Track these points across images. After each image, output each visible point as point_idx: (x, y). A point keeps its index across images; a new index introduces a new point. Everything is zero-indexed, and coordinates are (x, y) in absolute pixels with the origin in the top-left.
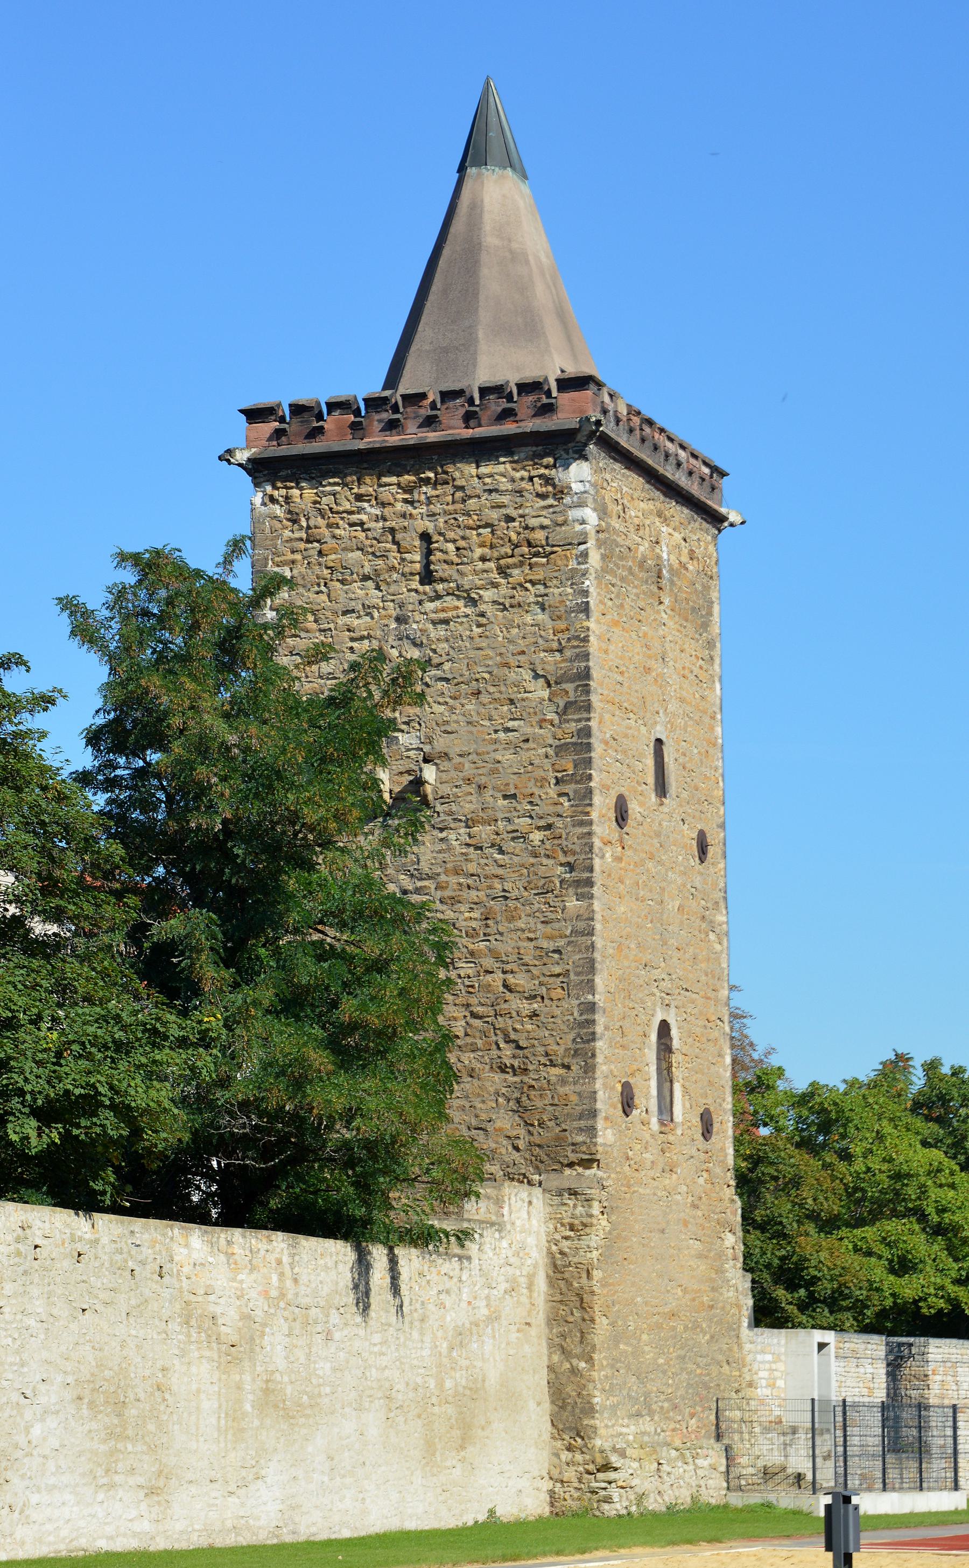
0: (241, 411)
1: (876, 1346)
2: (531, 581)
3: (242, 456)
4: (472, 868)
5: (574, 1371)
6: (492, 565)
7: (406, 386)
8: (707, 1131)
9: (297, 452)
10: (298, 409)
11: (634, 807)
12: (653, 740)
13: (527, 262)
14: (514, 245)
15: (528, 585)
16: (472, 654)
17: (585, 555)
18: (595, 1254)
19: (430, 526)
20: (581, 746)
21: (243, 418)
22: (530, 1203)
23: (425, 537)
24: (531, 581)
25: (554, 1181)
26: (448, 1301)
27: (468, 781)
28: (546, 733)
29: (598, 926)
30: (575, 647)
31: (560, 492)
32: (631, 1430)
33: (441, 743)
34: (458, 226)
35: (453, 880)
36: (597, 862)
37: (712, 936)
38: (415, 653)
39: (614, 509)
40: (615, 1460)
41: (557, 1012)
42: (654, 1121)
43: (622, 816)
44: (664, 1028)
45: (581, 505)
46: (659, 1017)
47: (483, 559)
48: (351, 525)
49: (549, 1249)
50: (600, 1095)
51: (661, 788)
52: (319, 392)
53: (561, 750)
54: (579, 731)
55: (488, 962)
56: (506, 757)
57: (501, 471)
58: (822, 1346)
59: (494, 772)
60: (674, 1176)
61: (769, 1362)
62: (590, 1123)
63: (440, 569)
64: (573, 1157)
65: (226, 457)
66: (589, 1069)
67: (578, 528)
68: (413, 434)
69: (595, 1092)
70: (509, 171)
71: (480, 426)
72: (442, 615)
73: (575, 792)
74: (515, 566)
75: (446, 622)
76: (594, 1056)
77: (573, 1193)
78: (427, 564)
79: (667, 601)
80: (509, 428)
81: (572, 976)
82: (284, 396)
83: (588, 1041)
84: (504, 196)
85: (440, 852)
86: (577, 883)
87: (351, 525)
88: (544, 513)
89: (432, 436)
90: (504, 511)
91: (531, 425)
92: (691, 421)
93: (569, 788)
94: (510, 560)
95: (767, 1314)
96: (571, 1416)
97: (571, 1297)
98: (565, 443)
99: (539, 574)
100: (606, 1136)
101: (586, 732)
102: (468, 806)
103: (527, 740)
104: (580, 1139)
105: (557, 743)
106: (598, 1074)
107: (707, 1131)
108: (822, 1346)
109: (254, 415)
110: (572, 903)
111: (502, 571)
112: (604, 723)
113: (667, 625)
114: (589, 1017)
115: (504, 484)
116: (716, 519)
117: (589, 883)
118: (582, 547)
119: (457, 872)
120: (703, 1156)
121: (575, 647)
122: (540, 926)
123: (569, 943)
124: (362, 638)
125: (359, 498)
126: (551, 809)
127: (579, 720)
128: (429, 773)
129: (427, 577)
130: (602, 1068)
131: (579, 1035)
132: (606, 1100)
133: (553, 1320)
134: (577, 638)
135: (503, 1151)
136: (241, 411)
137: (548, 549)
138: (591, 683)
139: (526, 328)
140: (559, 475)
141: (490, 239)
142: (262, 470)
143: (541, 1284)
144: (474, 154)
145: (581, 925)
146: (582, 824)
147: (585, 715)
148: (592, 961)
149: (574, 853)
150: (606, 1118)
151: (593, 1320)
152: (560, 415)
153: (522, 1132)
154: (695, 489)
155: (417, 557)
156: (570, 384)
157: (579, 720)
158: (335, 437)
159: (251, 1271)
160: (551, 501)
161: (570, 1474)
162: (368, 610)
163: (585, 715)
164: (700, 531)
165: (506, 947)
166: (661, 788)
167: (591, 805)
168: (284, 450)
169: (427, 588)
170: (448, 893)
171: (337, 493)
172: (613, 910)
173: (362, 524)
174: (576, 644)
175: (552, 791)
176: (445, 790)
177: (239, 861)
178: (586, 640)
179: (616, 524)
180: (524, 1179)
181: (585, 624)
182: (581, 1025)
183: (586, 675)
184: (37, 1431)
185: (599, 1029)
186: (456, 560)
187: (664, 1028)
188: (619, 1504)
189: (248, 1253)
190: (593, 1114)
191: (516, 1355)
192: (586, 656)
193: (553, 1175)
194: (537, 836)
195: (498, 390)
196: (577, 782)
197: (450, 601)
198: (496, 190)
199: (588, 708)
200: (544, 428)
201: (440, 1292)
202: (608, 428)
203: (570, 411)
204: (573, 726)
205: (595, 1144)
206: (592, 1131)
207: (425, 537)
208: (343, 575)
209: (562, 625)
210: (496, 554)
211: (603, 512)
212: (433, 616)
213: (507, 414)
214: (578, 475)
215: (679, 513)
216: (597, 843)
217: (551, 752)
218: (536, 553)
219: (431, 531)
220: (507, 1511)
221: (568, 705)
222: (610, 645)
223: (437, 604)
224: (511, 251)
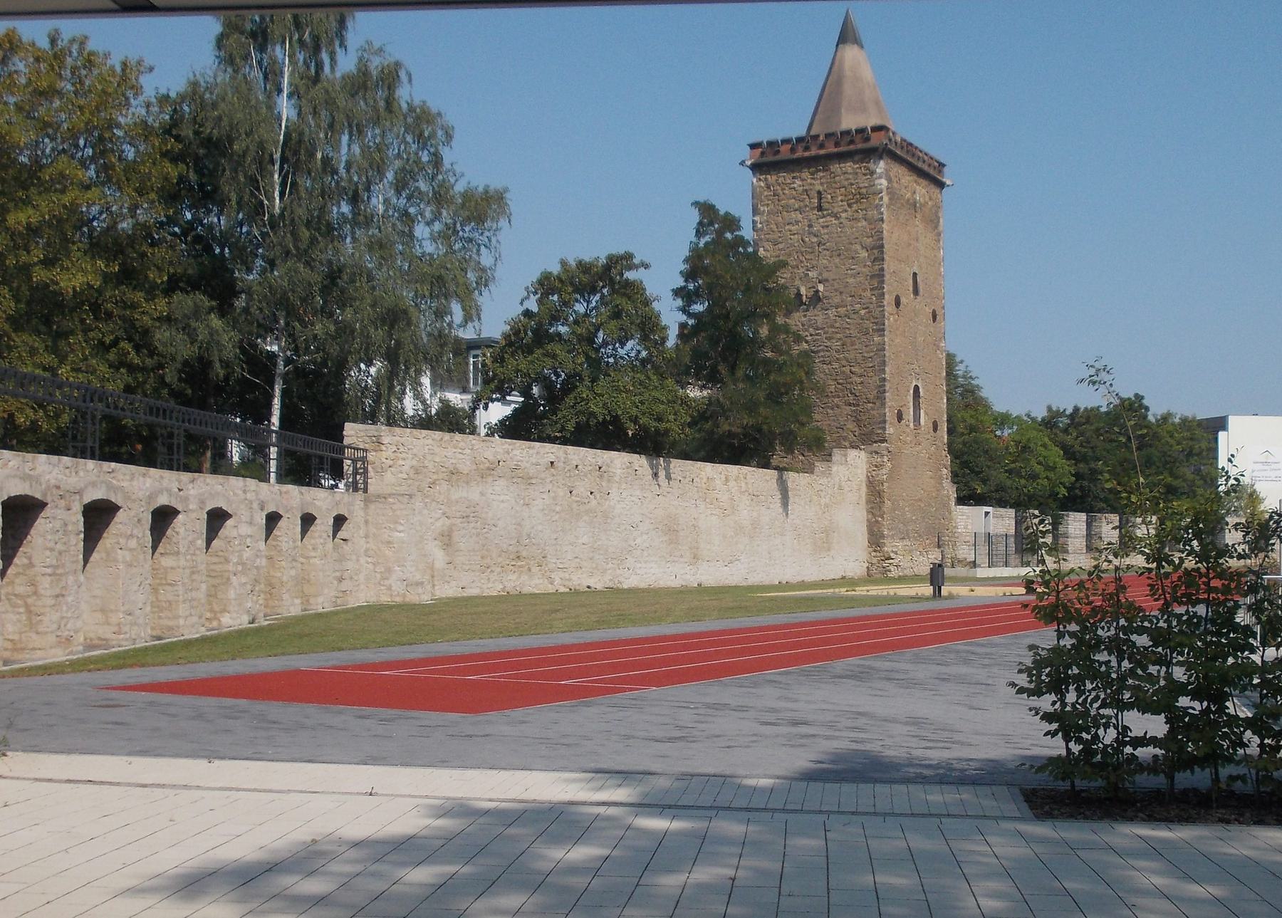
1: (1011, 512)
3: (749, 163)
5: (877, 521)
7: (812, 133)
8: (935, 429)
9: (771, 160)
10: (771, 144)
11: (903, 300)
17: (881, 198)
19: (821, 188)
20: (880, 276)
23: (819, 193)
26: (822, 494)
28: (865, 270)
31: (872, 173)
32: (900, 544)
33: (825, 275)
34: (835, 68)
35: (831, 330)
38: (815, 240)
39: (895, 180)
40: (892, 555)
43: (898, 303)
44: (916, 388)
45: (880, 177)
51: (916, 292)
52: (779, 136)
55: (844, 362)
56: (851, 280)
57: (849, 166)
58: (987, 513)
63: (825, 206)
65: (742, 163)
66: (883, 404)
68: (814, 151)
77: (877, 453)
78: (820, 203)
80: (852, 147)
82: (764, 138)
86: (879, 330)
89: (822, 152)
91: (860, 146)
92: (929, 143)
93: (875, 292)
95: (961, 501)
96: (875, 540)
97: (875, 494)
100: (890, 430)
101: (882, 269)
102: (837, 300)
107: (935, 429)
108: (987, 513)
109: (753, 146)
111: (850, 206)
112: (889, 265)
113: (918, 225)
115: (850, 170)
116: (941, 185)
117: (883, 330)
119: (833, 326)
128: (821, 287)
129: (820, 208)
130: (889, 404)
132: (890, 415)
133: (868, 502)
139: (862, 108)
140: (871, 165)
141: (848, 73)
142: (757, 168)
143: (864, 489)
144: (847, 35)
154: (932, 172)
156: (878, 129)
158: (785, 152)
161: (875, 561)
162: (797, 222)
164: (934, 190)
165: (851, 356)
166: (916, 292)
171: (784, 177)
172: (893, 342)
175: (868, 293)
176: (827, 294)
177: (691, 322)
179: (895, 185)
180: (856, 447)
183: (882, 246)
184: (638, 541)
187: (916, 388)
188: (894, 573)
190: (885, 422)
191: (851, 518)
194: (863, 312)
195: (848, 132)
197: (828, 218)
198: (851, 53)
199: (883, 260)
200: (866, 147)
202: (892, 147)
203: (876, 140)
206: (884, 429)
207: (819, 193)
208: (787, 208)
211: (889, 180)
213: (852, 142)
214: (881, 166)
215: (924, 182)
218: (862, 197)
220: (850, 574)
222: (892, 234)
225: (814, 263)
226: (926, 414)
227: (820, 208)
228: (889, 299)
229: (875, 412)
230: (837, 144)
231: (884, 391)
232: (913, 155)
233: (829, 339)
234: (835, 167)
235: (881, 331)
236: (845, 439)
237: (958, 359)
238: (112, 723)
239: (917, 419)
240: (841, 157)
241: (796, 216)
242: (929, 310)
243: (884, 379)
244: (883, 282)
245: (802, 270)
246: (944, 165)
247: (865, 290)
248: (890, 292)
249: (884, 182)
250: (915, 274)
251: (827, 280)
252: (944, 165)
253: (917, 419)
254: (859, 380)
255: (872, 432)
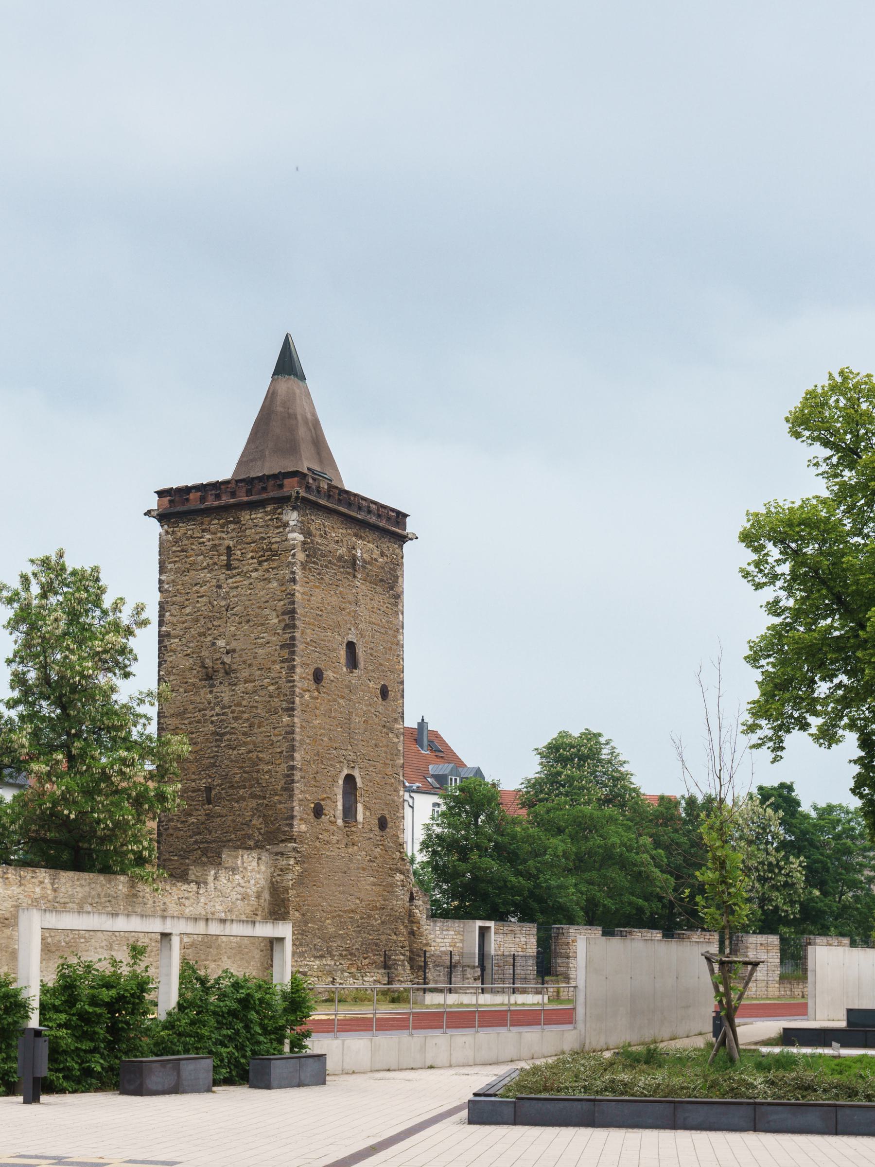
4: (244, 703)
6: (255, 561)
11: (329, 674)
13: (296, 418)
14: (291, 411)
18: (291, 883)
19: (231, 543)
20: (290, 646)
21: (156, 495)
22: (259, 859)
27: (244, 662)
29: (297, 730)
33: (234, 645)
35: (237, 709)
36: (297, 700)
37: (391, 735)
41: (278, 769)
42: (340, 822)
43: (318, 676)
44: (350, 780)
46: (346, 772)
47: (252, 558)
50: (297, 808)
53: (282, 647)
57: (258, 516)
59: (255, 657)
60: (356, 847)
63: (235, 563)
64: (283, 838)
66: (291, 797)
68: (226, 500)
70: (292, 377)
72: (235, 585)
78: (228, 560)
79: (359, 576)
80: (264, 496)
91: (272, 494)
99: (275, 564)
100: (300, 827)
101: (293, 638)
102: (245, 674)
104: (286, 829)
106: (295, 798)
109: (161, 494)
110: (286, 719)
112: (304, 634)
119: (239, 705)
124: (202, 596)
125: (203, 531)
126: (278, 675)
130: (298, 795)
134: (290, 594)
142: (163, 517)
145: (288, 729)
146: (290, 681)
148: (293, 746)
150: (301, 820)
151: (289, 913)
153: (263, 826)
155: (225, 558)
160: (281, 530)
164: (388, 546)
170: (235, 715)
178: (293, 595)
182: (288, 776)
183: (293, 611)
185: (296, 778)
187: (350, 780)
190: (292, 817)
192: (293, 603)
194: (271, 688)
197: (238, 578)
201: (179, 898)
203: (292, 487)
206: (291, 826)
207: (228, 548)
209: (284, 588)
211: (307, 533)
213: (264, 489)
216: (297, 690)
217: (278, 648)
223: (234, 580)
226: (366, 808)
227: (228, 566)
228: (302, 674)
230: (249, 493)
231: (293, 781)
232: (360, 508)
233: (236, 719)
234: (246, 517)
235: (290, 710)
236: (250, 837)
237: (602, 740)
238: (16, 1157)
239: (349, 812)
240: (252, 506)
241: (204, 575)
243: (293, 768)
244: (293, 653)
245: (209, 638)
247: (274, 662)
248: (304, 665)
249: (296, 537)
250: (351, 646)
251: (234, 651)
252: (406, 516)
253: (349, 812)
254: (266, 768)
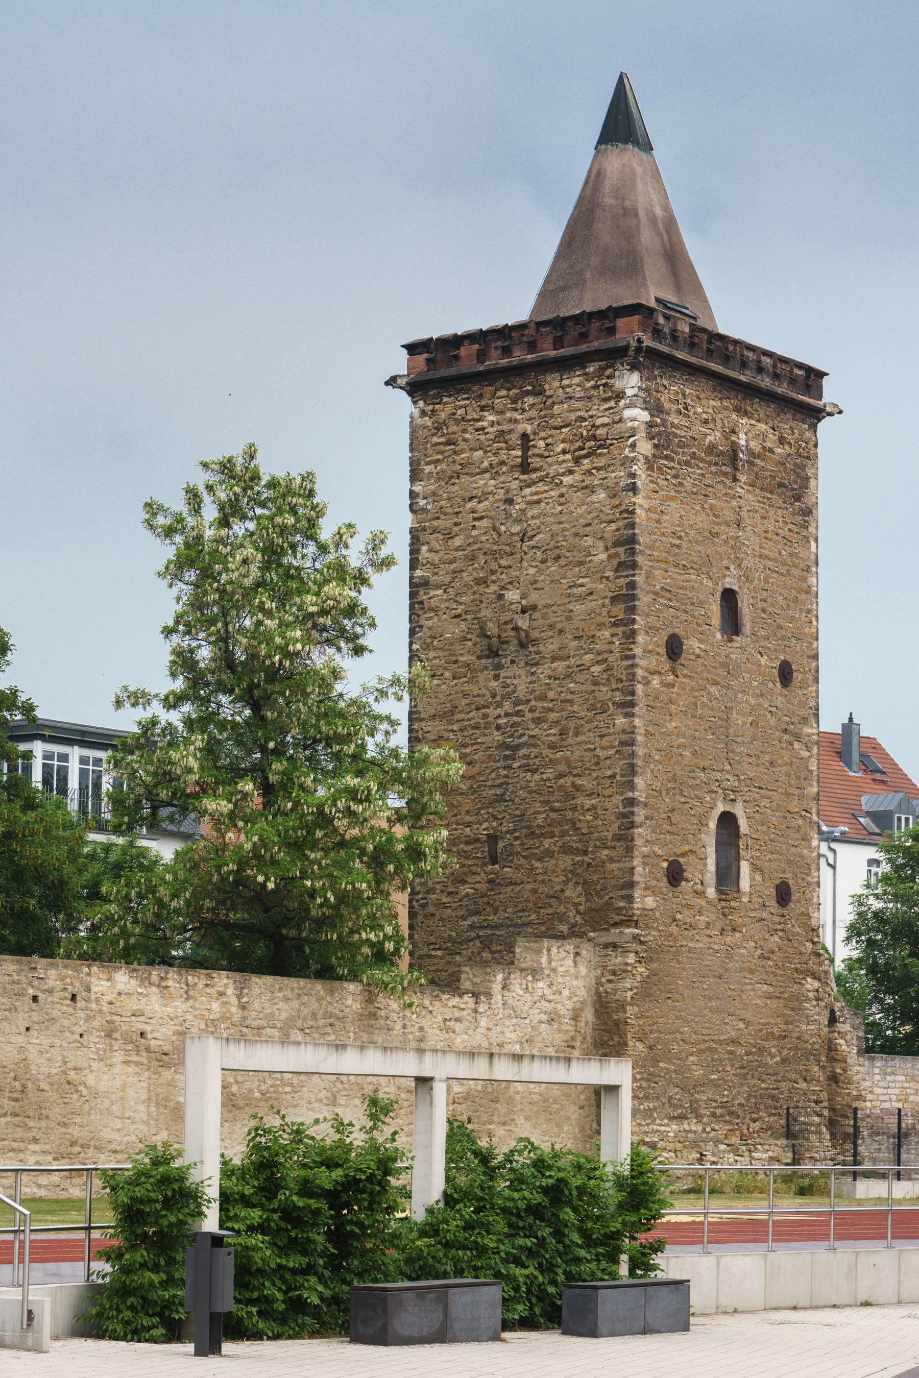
0: (403, 346)
2: (595, 468)
3: (402, 382)
4: (551, 694)
6: (569, 456)
11: (692, 644)
12: (720, 589)
13: (637, 215)
14: (627, 203)
15: (594, 471)
16: (555, 527)
18: (629, 994)
19: (529, 428)
20: (627, 598)
21: (405, 351)
22: (577, 954)
24: (595, 468)
25: (604, 938)
27: (551, 626)
29: (640, 738)
30: (625, 518)
33: (534, 597)
35: (540, 704)
36: (639, 689)
37: (796, 745)
41: (608, 805)
43: (674, 648)
44: (728, 821)
46: (721, 808)
47: (564, 452)
48: (477, 430)
49: (597, 989)
50: (639, 869)
53: (614, 600)
54: (627, 584)
57: (574, 382)
59: (569, 619)
60: (738, 935)
61: (901, 1081)
62: (630, 892)
63: (535, 462)
64: (617, 919)
66: (630, 850)
67: (629, 424)
68: (520, 356)
69: (633, 868)
71: (563, 347)
72: (535, 498)
73: (623, 633)
74: (586, 456)
75: (539, 502)
76: (633, 840)
77: (615, 946)
78: (525, 456)
80: (584, 348)
81: (618, 777)
83: (628, 829)
84: (624, 165)
85: (531, 683)
87: (477, 430)
88: (606, 413)
90: (579, 414)
93: (620, 630)
94: (582, 452)
98: (621, 358)
99: (602, 462)
100: (644, 901)
101: (632, 585)
103: (591, 593)
104: (622, 904)
105: (611, 594)
109: (412, 348)
110: (620, 721)
112: (650, 577)
114: (630, 809)
118: (632, 440)
119: (542, 698)
120: (776, 919)
121: (625, 518)
122: (598, 739)
123: (617, 752)
124: (482, 518)
126: (607, 647)
127: (627, 576)
130: (641, 848)
131: (622, 824)
134: (626, 511)
135: (570, 914)
136: (403, 346)
137: (609, 442)
138: (637, 547)
142: (416, 388)
145: (625, 737)
146: (627, 658)
147: (631, 572)
149: (622, 681)
151: (626, 1044)
152: (618, 336)
155: (519, 453)
157: (627, 576)
159: (187, 999)
162: (486, 495)
163: (631, 572)
167: (634, 643)
168: (433, 375)
169: (526, 477)
170: (537, 714)
173: (483, 429)
174: (626, 515)
178: (632, 512)
181: (634, 500)
182: (624, 815)
185: (638, 819)
186: (546, 454)
187: (728, 821)
189: (183, 986)
190: (631, 885)
192: (632, 525)
193: (603, 933)
194: (596, 669)
196: (625, 625)
197: (541, 487)
201: (445, 1020)
204: (623, 581)
205: (632, 908)
206: (630, 899)
210: (572, 448)
211: (656, 409)
212: (529, 498)
213: (584, 336)
216: (640, 672)
217: (607, 601)
219: (529, 432)
221: (621, 564)
224: (624, 208)
225: (514, 573)
226: (755, 868)
227: (525, 467)
229: (614, 866)
230: (558, 343)
231: (632, 825)
232: (744, 364)
233: (537, 721)
234: (552, 383)
235: (628, 706)
236: (561, 918)
239: (727, 876)
240: (564, 365)
241: (484, 482)
242: (769, 663)
243: (632, 802)
244: (632, 610)
245: (493, 588)
246: (821, 375)
247: (601, 626)
248: (651, 629)
249: (637, 415)
251: (534, 608)
252: (821, 375)
253: (727, 876)
254: (588, 803)
255: (608, 904)
